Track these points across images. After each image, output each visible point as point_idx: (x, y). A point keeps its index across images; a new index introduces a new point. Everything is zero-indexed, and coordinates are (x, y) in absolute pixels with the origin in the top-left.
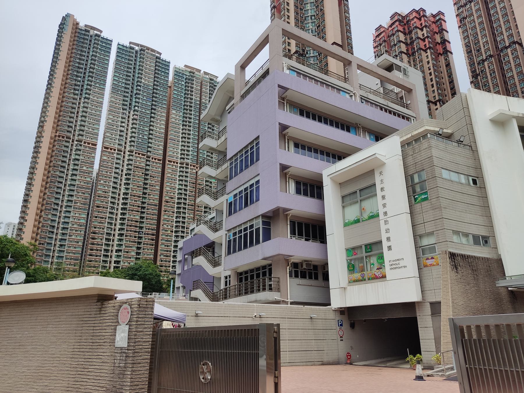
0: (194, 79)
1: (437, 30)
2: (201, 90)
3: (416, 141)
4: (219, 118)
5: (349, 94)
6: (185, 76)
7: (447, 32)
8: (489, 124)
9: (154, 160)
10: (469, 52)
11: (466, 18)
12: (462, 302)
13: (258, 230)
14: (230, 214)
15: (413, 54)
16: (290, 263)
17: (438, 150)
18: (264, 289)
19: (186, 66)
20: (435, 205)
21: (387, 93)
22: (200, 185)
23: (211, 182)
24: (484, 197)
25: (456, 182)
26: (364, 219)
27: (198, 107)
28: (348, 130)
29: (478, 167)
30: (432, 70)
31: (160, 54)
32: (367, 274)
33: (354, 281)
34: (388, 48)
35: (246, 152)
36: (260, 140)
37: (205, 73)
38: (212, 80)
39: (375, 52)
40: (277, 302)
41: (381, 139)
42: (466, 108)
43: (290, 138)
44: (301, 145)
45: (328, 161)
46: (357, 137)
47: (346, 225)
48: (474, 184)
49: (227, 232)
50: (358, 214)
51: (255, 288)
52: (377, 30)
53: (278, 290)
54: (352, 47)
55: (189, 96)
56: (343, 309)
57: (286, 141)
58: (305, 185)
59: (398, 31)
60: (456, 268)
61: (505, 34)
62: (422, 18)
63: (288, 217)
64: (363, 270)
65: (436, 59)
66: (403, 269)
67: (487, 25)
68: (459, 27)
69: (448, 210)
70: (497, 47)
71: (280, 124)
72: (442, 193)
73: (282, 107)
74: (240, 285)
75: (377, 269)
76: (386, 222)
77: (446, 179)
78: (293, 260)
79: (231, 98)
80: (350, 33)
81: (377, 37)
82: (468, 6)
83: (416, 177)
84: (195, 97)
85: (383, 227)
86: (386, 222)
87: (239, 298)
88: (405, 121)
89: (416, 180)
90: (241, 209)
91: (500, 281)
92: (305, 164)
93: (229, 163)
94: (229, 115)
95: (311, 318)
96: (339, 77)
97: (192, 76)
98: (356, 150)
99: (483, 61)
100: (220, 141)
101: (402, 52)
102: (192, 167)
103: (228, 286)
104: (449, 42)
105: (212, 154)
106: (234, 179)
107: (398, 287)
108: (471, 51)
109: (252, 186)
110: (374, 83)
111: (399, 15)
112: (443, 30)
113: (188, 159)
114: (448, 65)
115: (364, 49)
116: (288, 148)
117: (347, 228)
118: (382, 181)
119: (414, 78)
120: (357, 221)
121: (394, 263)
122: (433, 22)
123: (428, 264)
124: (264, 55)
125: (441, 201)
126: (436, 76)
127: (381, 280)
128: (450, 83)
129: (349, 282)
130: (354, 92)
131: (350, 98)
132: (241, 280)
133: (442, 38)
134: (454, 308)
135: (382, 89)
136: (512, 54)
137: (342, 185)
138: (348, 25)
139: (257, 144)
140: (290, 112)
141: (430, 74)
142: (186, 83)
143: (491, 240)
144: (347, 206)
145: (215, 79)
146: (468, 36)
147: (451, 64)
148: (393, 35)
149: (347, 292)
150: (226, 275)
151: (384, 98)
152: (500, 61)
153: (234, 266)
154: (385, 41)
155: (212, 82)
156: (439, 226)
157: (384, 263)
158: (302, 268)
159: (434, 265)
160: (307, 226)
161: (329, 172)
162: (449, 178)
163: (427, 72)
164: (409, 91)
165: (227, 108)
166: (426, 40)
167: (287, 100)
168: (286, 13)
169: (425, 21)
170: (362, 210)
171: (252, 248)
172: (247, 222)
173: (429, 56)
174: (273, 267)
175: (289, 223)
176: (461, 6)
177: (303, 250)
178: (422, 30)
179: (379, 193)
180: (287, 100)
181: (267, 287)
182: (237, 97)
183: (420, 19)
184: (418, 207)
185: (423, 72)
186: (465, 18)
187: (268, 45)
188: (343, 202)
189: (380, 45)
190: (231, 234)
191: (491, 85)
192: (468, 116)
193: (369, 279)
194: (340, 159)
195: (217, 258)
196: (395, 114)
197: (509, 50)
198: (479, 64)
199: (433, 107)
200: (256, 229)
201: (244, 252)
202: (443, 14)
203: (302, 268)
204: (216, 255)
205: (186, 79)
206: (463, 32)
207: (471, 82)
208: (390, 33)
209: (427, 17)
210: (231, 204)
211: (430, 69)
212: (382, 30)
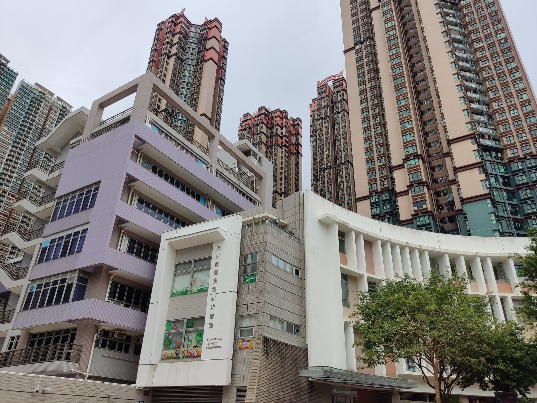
0: (44, 100)
2: (48, 114)
3: (257, 224)
4: (58, 150)
5: (206, 165)
6: (32, 95)
7: (301, 137)
8: (317, 224)
9: (10, 196)
10: (315, 159)
11: (317, 130)
12: (266, 390)
13: (70, 286)
14: (40, 261)
15: (271, 147)
16: (99, 330)
17: (273, 237)
18: (59, 358)
19: (37, 84)
20: (260, 288)
21: (241, 174)
22: (14, 219)
23: (30, 219)
25: (282, 270)
26: (193, 292)
27: (39, 131)
28: (198, 199)
29: (302, 260)
30: (283, 165)
31: (8, 62)
32: (183, 351)
33: (168, 358)
34: (251, 135)
35: (82, 194)
36: (101, 185)
37: (59, 99)
38: (65, 108)
39: (239, 135)
40: (72, 375)
41: (227, 214)
42: (301, 205)
43: (135, 192)
44: (147, 203)
45: (171, 225)
46: (205, 207)
47: (173, 295)
48: (296, 274)
49: (30, 282)
50: (188, 285)
51: (48, 355)
52: (245, 116)
53: (77, 361)
54: (219, 124)
55: (31, 117)
56: (148, 389)
57: (131, 194)
58: (140, 244)
59: (262, 123)
60: (267, 354)
61: (343, 154)
62: (284, 119)
63: (111, 277)
64: (179, 347)
65: (288, 157)
66: (219, 349)
67: (331, 142)
68: (311, 136)
69: (270, 295)
70: (336, 162)
71: (127, 174)
72: (269, 277)
73: (135, 159)
74: (29, 350)
75: (194, 347)
77: (274, 265)
78: (104, 327)
79: (79, 133)
80: (221, 110)
81: (243, 122)
82: (320, 122)
83: (249, 257)
84: (39, 120)
85: (209, 303)
86: (213, 298)
87: (22, 367)
88: (252, 203)
89: (249, 261)
90: (55, 258)
91: (303, 371)
92: (145, 222)
93: (56, 202)
94: (71, 150)
95: (109, 397)
96: (201, 147)
97: (41, 97)
98: (201, 220)
99: (324, 169)
100: (52, 176)
101: (262, 142)
102: (10, 196)
103: (13, 349)
104: (301, 146)
105: (41, 187)
106: (57, 222)
108: (316, 159)
109: (77, 233)
110: (232, 162)
111: (266, 110)
112: (298, 134)
113: (8, 186)
114: (297, 165)
115: (230, 129)
116: (131, 201)
117: (173, 298)
118: (218, 255)
119: (267, 168)
120: (185, 293)
121: (212, 342)
122: (292, 125)
123: (243, 346)
124: (129, 102)
125: (266, 285)
127: (195, 359)
129: (162, 359)
130: (211, 164)
131: (206, 168)
132: (32, 344)
133: (296, 140)
134: (257, 395)
135: (237, 169)
136: (345, 170)
137: (178, 252)
138: (220, 102)
139: (97, 189)
140: (143, 166)
141: (282, 168)
142: (31, 102)
143: (301, 330)
144: (179, 275)
145: (68, 108)
146: (316, 145)
147: (299, 165)
148: (258, 125)
150: (13, 335)
151: (237, 178)
152: (336, 173)
153: (27, 325)
154: (249, 128)
155: (64, 110)
156: (260, 309)
157: (202, 341)
158: (113, 338)
159: (248, 348)
160: (131, 290)
161: (169, 236)
162: (276, 264)
163: (279, 166)
164: (260, 178)
165: (72, 142)
166: (284, 138)
167: (141, 152)
168: (164, 71)
169: (286, 122)
170: (193, 282)
171: (57, 306)
172: (59, 274)
173: (284, 153)
174: (77, 332)
175: (110, 284)
176: (315, 120)
177: (117, 316)
178: (282, 128)
179: (213, 268)
180: (141, 152)
181: (64, 356)
182: (87, 133)
183: (282, 119)
184: (245, 287)
185: (276, 165)
186: (316, 130)
187: (135, 94)
188: (176, 270)
189: (245, 130)
190: (35, 286)
191: (327, 191)
192: (302, 212)
193: (183, 357)
194: (183, 225)
195: (8, 312)
196: (244, 195)
197: (344, 166)
198: (320, 171)
199: (278, 197)
200: (68, 285)
201: (46, 310)
202: (301, 121)
203: (113, 338)
204: (8, 308)
205: (33, 98)
206: (313, 141)
207: (312, 185)
210: (44, 249)
211: (282, 164)
212: (249, 117)
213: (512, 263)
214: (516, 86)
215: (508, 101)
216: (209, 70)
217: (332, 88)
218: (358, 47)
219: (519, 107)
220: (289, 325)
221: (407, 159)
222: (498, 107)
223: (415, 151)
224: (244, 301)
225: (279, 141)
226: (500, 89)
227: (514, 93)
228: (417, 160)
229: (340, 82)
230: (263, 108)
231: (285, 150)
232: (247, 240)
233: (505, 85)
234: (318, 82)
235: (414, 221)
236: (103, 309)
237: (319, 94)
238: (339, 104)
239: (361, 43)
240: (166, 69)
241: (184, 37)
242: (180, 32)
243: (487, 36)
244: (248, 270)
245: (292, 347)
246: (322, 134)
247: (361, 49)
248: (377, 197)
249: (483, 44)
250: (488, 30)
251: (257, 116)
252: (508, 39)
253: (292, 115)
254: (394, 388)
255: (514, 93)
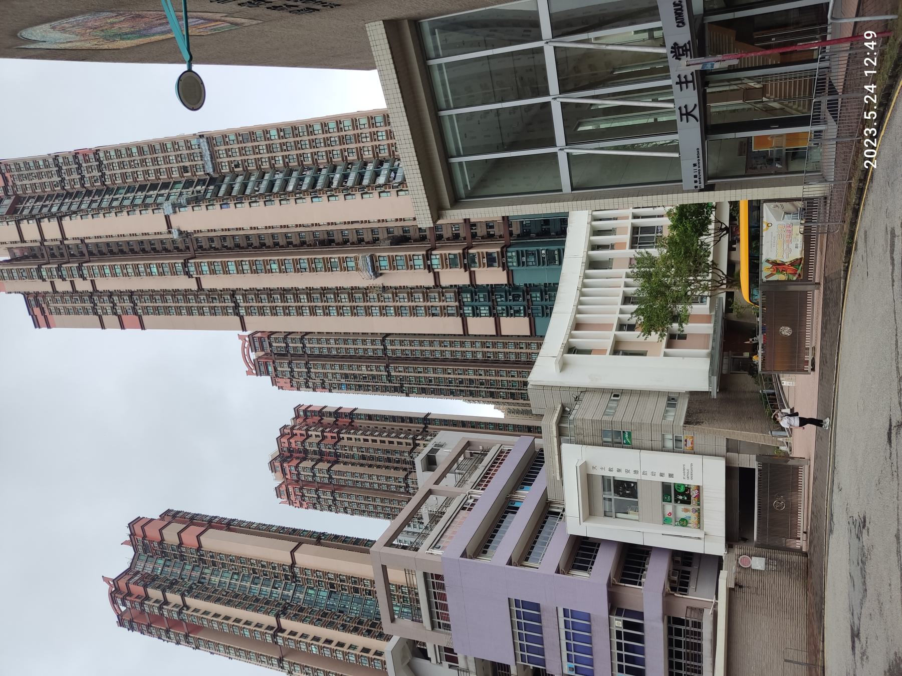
1: (317, 418)
24: (631, 392)
29: (603, 391)
30: (370, 438)
52: (279, 495)
53: (701, 611)
59: (297, 467)
76: (644, 473)
82: (313, 375)
86: (644, 473)
92: (554, 550)
99: (389, 375)
101: (329, 470)
107: (710, 477)
111: (275, 459)
114: (370, 417)
122: (305, 420)
126: (380, 435)
128: (394, 421)
143: (672, 396)
148: (299, 474)
149: (709, 536)
154: (301, 489)
164: (469, 444)
168: (209, 617)
169: (300, 429)
177: (656, 574)
183: (294, 435)
184: (634, 443)
186: (323, 383)
189: (303, 496)
193: (699, 505)
202: (300, 406)
208: (295, 478)
209: (294, 426)
212: (283, 488)
213: (406, 22)
214: (346, 128)
215: (364, 140)
216: (214, 541)
217: (261, 354)
218: (242, 311)
219: (375, 130)
220: (669, 405)
221: (430, 268)
222: (371, 152)
223: (421, 257)
224: (648, 444)
225: (329, 441)
226: (346, 146)
227: (356, 132)
228: (433, 257)
229: (256, 341)
230: (272, 464)
231: (346, 433)
232: (587, 440)
233: (342, 140)
234: (249, 373)
235: (511, 268)
236: (649, 594)
237: (268, 374)
238: (290, 345)
239: (237, 307)
240: (206, 613)
241: (154, 580)
242: (145, 587)
243: (269, 149)
244: (619, 439)
245: (689, 403)
246: (333, 374)
247: (247, 308)
248: (465, 308)
249: (279, 155)
250: (261, 148)
251: (284, 474)
252: (280, 129)
253: (287, 418)
254: (723, 318)
255: (356, 132)
